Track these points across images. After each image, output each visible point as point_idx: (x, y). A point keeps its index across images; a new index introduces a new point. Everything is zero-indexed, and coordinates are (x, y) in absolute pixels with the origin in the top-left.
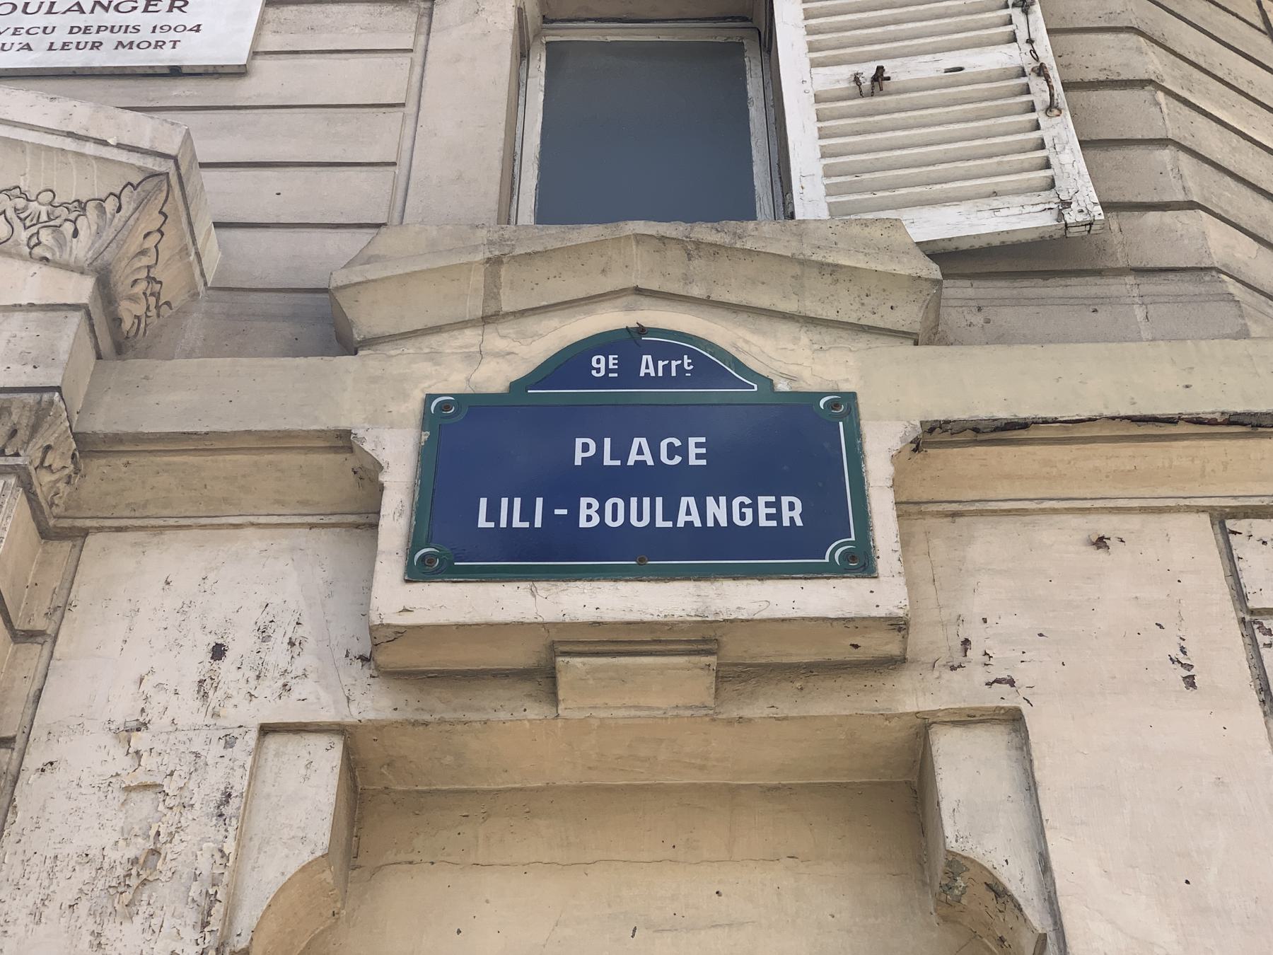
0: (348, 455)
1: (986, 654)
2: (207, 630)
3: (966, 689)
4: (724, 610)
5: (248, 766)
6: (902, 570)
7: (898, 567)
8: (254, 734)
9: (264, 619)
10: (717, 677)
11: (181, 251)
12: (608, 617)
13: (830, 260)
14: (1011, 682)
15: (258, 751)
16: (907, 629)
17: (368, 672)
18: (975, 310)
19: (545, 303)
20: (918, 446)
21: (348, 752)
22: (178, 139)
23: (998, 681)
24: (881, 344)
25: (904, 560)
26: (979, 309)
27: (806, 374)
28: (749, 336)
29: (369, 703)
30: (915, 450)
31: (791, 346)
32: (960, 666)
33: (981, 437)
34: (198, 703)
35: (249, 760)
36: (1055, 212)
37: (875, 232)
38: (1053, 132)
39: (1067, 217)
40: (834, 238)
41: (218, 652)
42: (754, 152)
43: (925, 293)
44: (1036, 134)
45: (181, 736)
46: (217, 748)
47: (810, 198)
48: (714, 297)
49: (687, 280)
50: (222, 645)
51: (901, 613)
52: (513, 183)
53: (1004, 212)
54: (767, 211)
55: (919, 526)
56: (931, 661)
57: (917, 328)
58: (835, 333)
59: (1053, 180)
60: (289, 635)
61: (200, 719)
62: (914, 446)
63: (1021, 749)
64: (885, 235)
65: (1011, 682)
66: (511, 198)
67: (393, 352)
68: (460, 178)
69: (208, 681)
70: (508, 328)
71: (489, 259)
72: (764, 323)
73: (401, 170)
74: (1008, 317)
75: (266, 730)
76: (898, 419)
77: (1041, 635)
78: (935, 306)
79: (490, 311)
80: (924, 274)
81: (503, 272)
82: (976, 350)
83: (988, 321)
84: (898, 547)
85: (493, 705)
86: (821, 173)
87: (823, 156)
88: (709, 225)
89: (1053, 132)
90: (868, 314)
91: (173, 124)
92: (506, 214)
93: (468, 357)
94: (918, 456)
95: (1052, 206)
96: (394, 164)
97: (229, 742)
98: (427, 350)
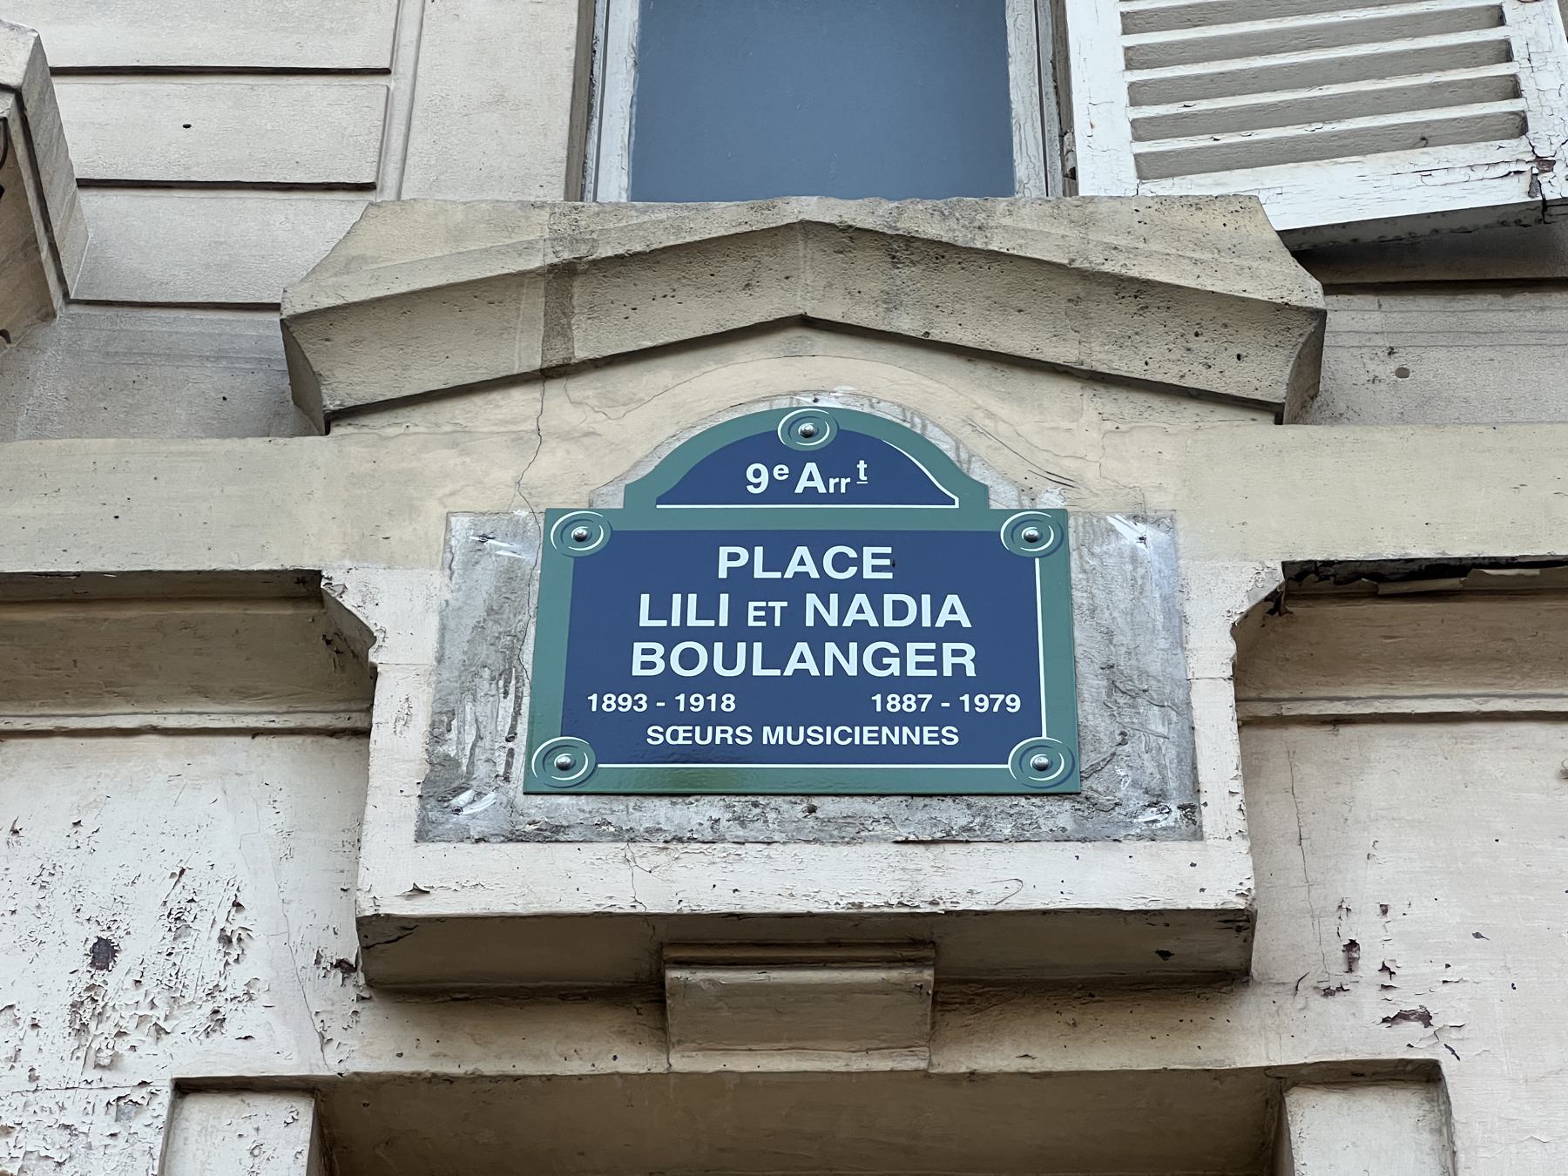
0: (315, 611)
1: (1384, 968)
2: (84, 916)
3: (1353, 1030)
4: (946, 895)
5: (157, 1153)
6: (1243, 826)
7: (1238, 822)
8: (166, 1096)
9: (178, 898)
10: (934, 1002)
11: (26, 244)
12: (754, 906)
13: (1134, 272)
14: (1426, 1018)
15: (173, 1107)
16: (1251, 929)
17: (353, 993)
18: (1383, 354)
19: (648, 344)
20: (1275, 604)
21: (322, 1125)
22: (23, 56)
23: (1403, 1016)
24: (1219, 420)
25: (1250, 808)
26: (1391, 352)
27: (1091, 474)
28: (995, 406)
29: (356, 1044)
30: (1271, 612)
31: (1065, 424)
32: (1341, 989)
33: (1384, 589)
34: (72, 1043)
35: (158, 1142)
36: (1525, 181)
37: (1213, 222)
38: (1528, 31)
39: (1546, 189)
40: (1141, 230)
41: (103, 954)
42: (1011, 38)
43: (1297, 332)
44: (1496, 34)
45: (45, 1099)
46: (104, 1123)
47: (1106, 157)
48: (936, 335)
49: (891, 302)
50: (108, 942)
51: (1241, 904)
52: (591, 95)
53: (1440, 177)
54: (1032, 152)
55: (1277, 740)
56: (1293, 980)
57: (1278, 394)
58: (1140, 399)
59: (1525, 120)
60: (221, 924)
61: (76, 1071)
62: (1271, 605)
63: (1440, 1132)
64: (1231, 227)
65: (1426, 1018)
66: (589, 123)
67: (391, 431)
68: (499, 100)
69: (89, 1005)
70: (585, 388)
71: (553, 266)
72: (1020, 381)
73: (398, 84)
74: (1439, 367)
75: (185, 1088)
76: (1245, 557)
77: (1477, 935)
78: (1310, 358)
79: (556, 359)
80: (1295, 300)
81: (577, 291)
82: (1381, 435)
83: (1403, 373)
84: (1237, 786)
85: (561, 1048)
86: (1125, 99)
87: (1130, 66)
88: (929, 203)
89: (1528, 31)
90: (1197, 368)
91: (12, 27)
92: (578, 175)
93: (518, 439)
94: (1277, 620)
95: (1526, 168)
96: (385, 72)
97: (123, 1107)
98: (448, 428)
